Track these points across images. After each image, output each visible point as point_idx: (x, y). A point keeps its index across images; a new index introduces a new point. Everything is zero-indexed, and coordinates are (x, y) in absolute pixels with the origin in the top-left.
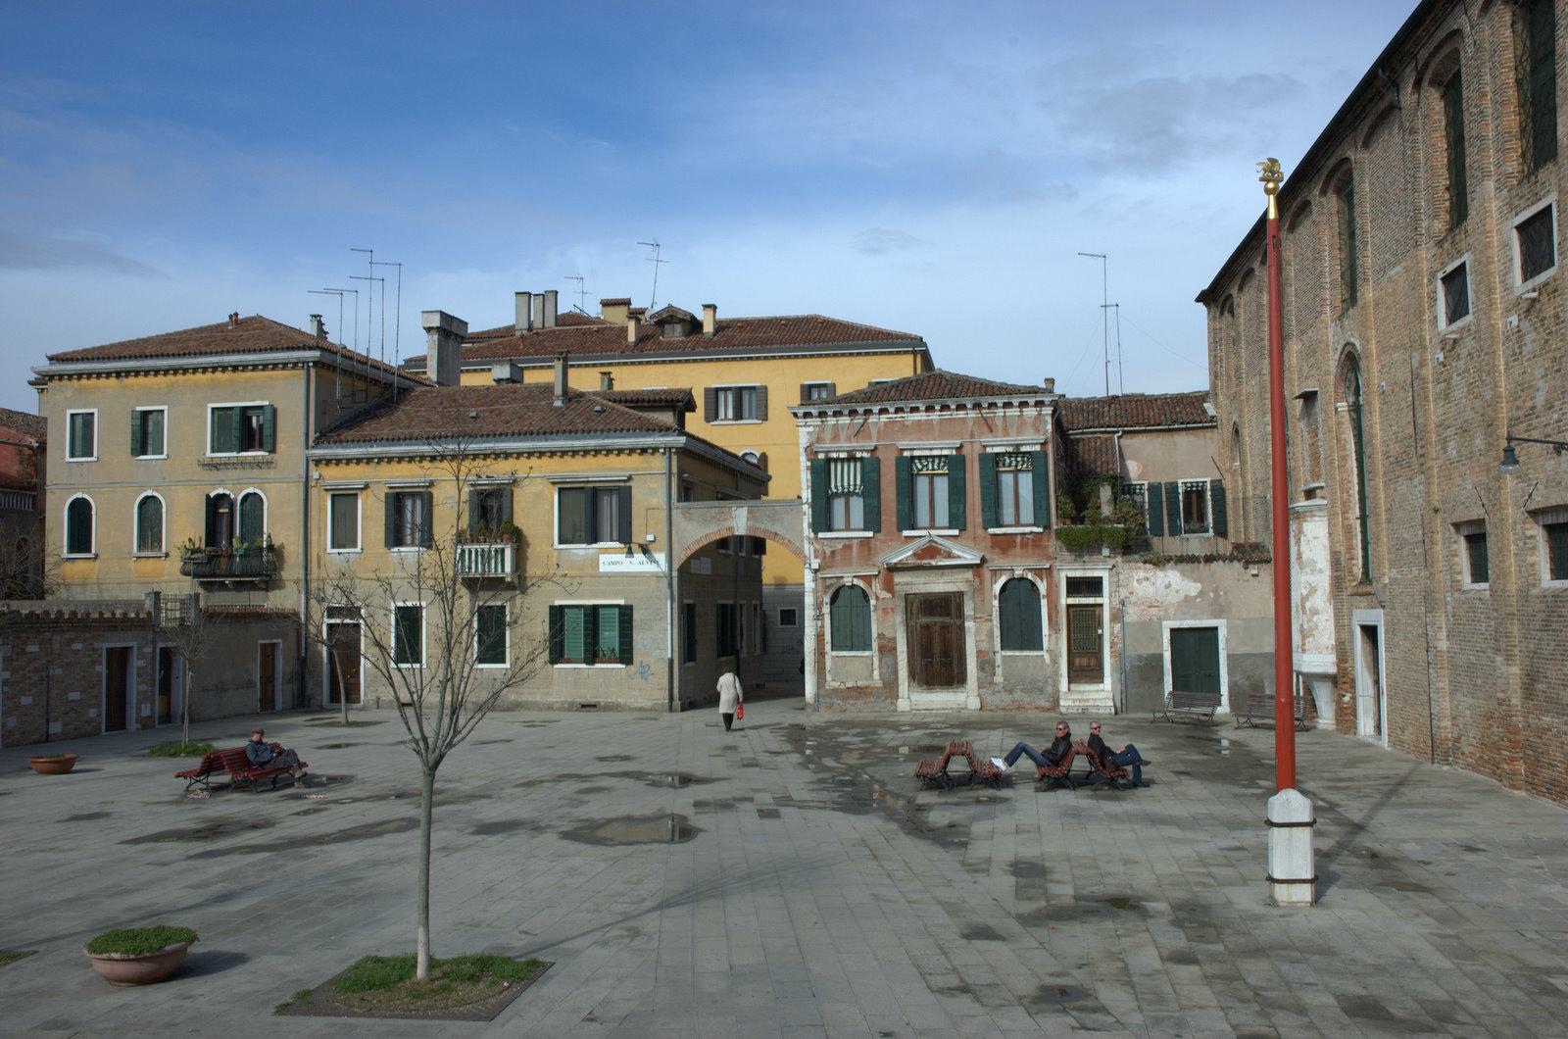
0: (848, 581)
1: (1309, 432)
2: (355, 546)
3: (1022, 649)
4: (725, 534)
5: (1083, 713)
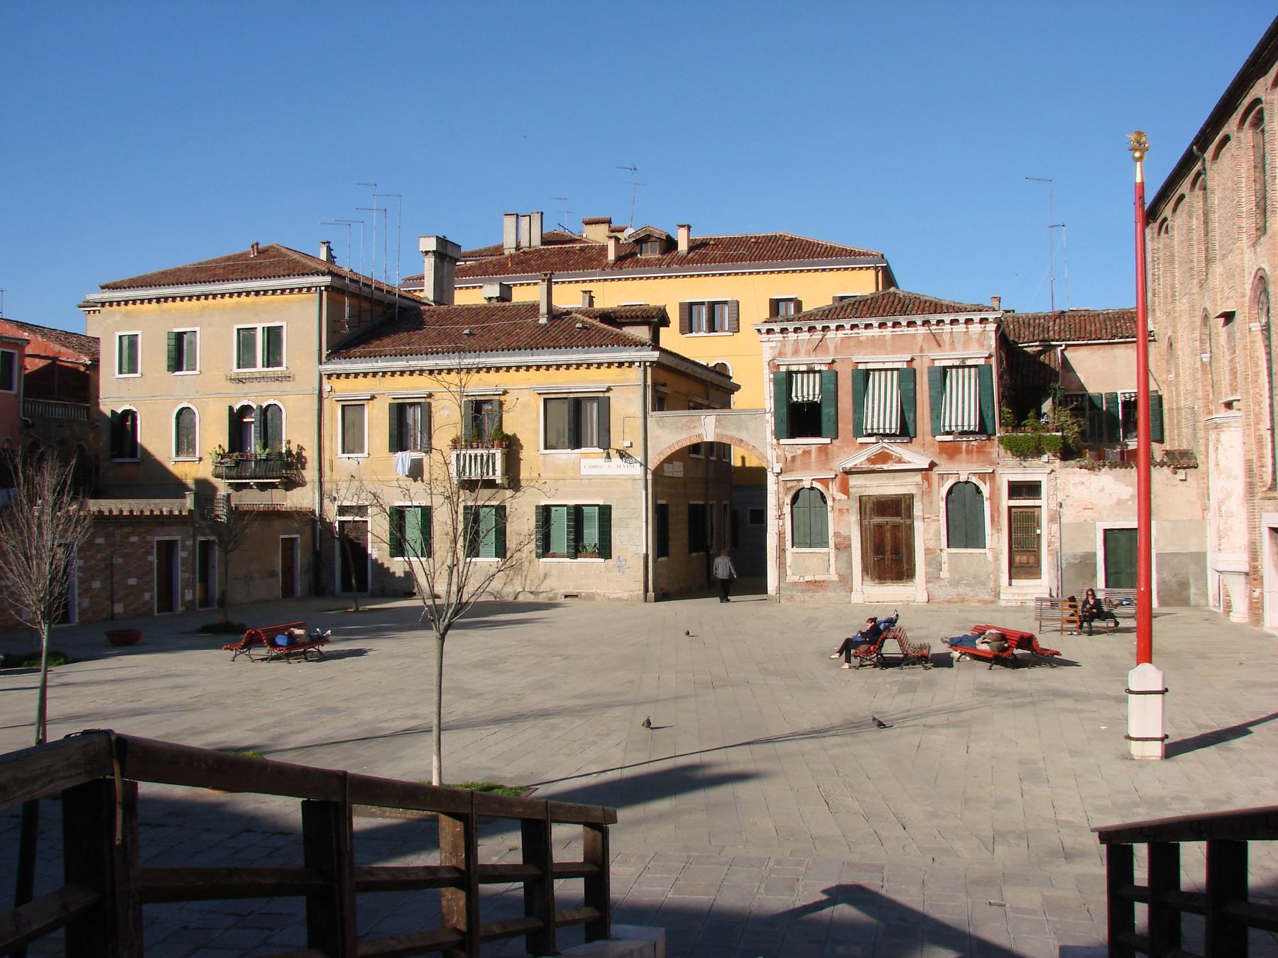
0: (807, 484)
1: (1228, 348)
2: (362, 452)
3: (966, 547)
4: (695, 441)
5: (1022, 606)
